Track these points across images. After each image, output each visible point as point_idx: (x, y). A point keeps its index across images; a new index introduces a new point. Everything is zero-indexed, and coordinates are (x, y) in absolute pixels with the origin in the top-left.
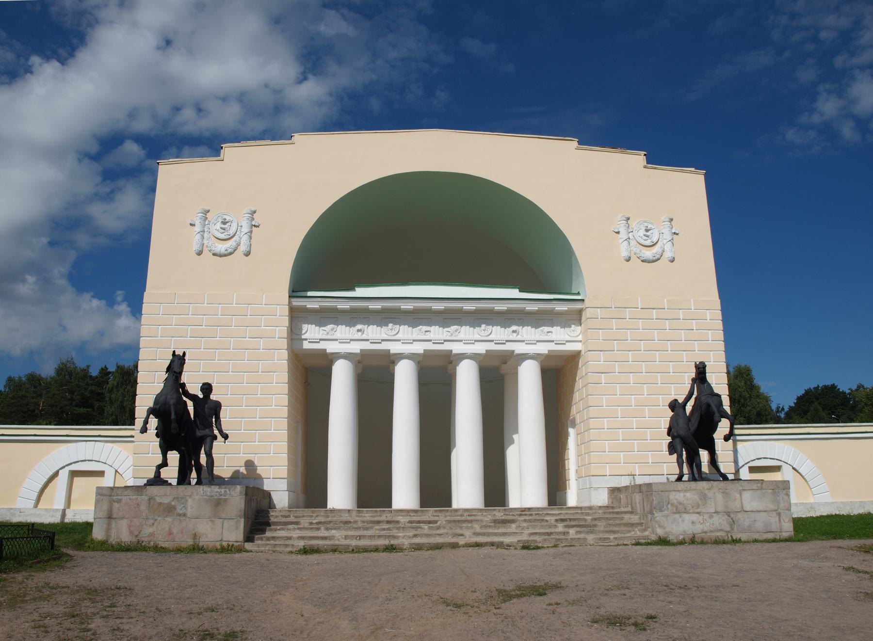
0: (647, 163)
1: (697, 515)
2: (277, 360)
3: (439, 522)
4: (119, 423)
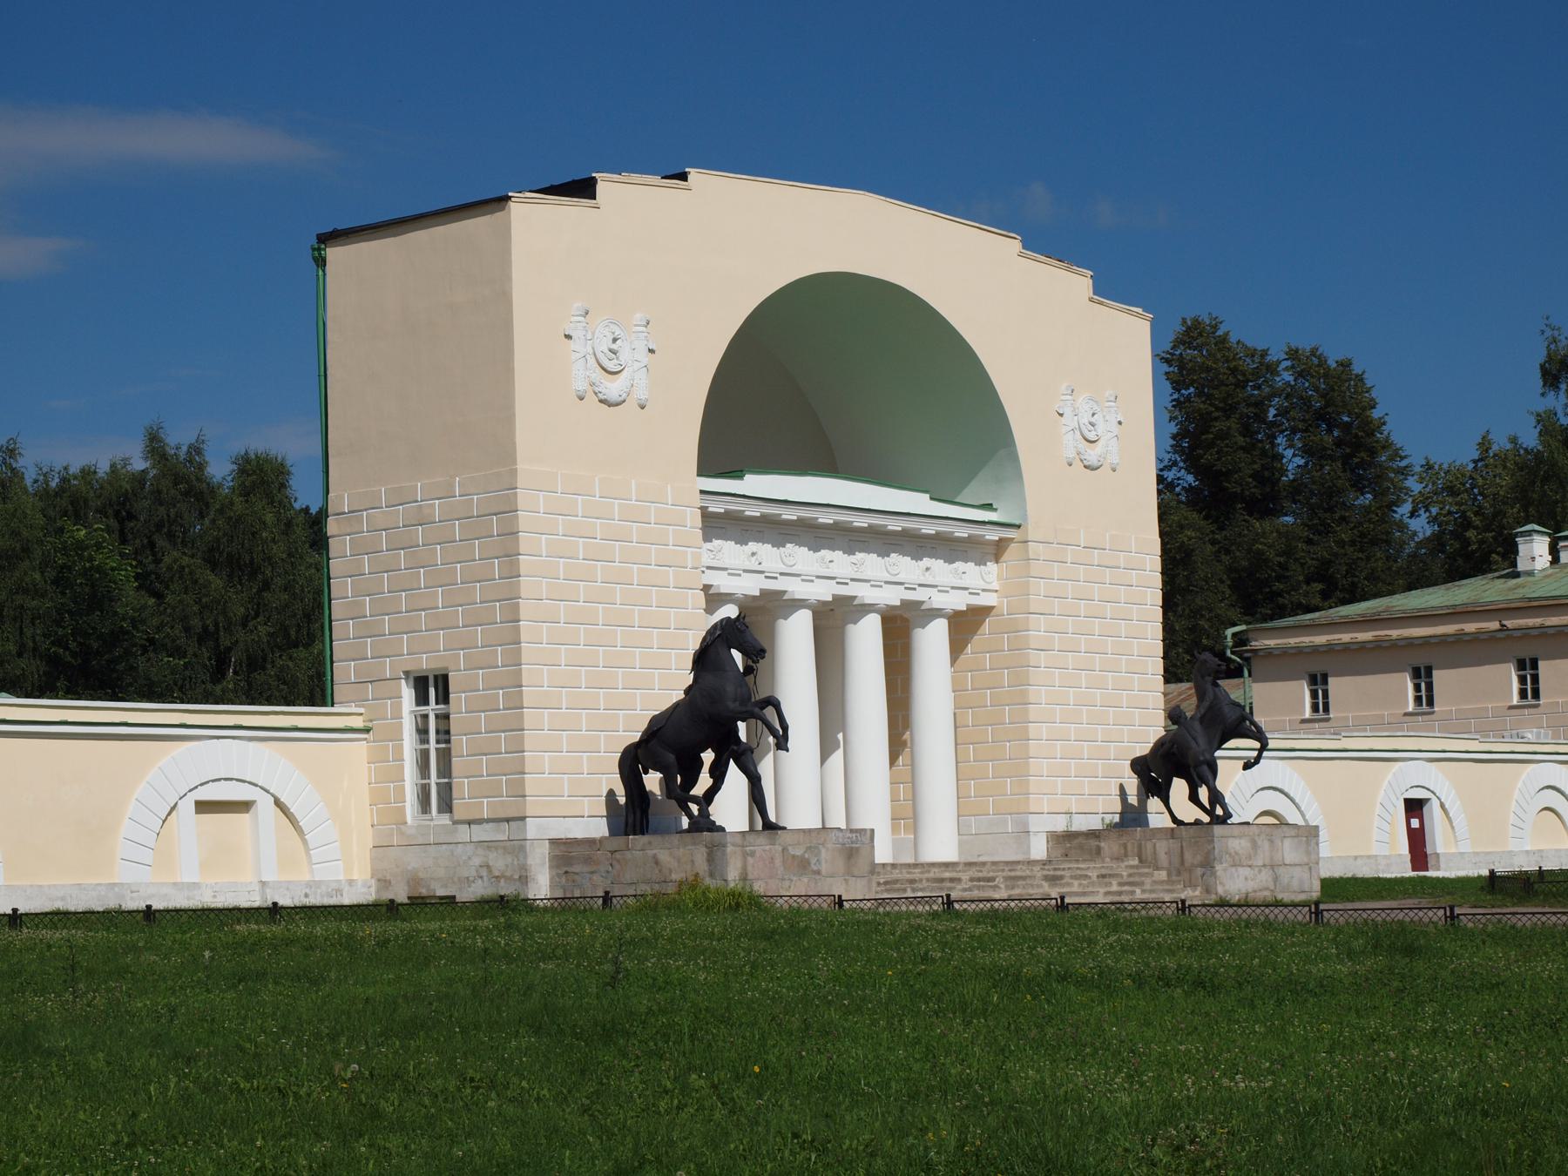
0: (1094, 294)
1: (1249, 869)
2: (692, 609)
3: (997, 879)
4: (226, 701)
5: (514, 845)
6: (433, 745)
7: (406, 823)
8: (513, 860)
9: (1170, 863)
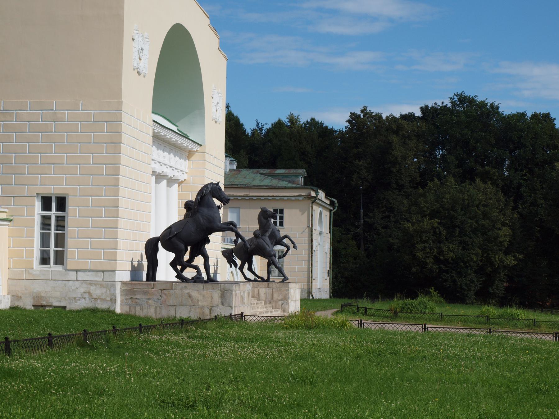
5: (108, 284)
6: (53, 231)
7: (33, 268)
8: (107, 291)
9: (266, 298)
